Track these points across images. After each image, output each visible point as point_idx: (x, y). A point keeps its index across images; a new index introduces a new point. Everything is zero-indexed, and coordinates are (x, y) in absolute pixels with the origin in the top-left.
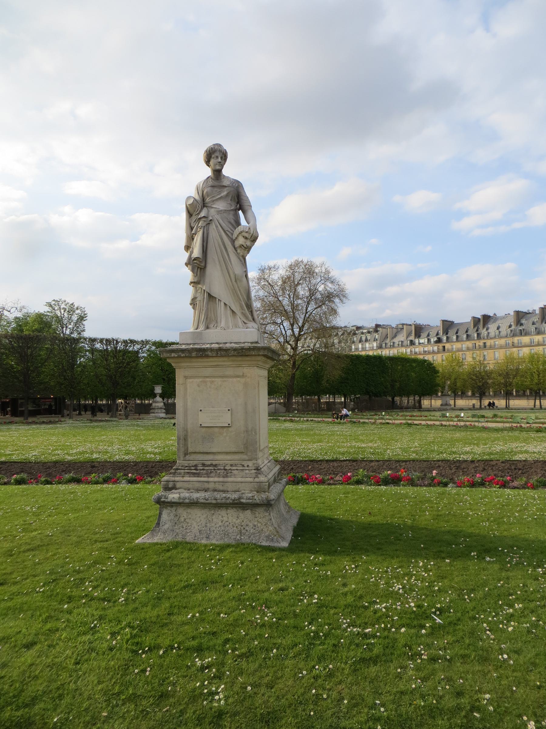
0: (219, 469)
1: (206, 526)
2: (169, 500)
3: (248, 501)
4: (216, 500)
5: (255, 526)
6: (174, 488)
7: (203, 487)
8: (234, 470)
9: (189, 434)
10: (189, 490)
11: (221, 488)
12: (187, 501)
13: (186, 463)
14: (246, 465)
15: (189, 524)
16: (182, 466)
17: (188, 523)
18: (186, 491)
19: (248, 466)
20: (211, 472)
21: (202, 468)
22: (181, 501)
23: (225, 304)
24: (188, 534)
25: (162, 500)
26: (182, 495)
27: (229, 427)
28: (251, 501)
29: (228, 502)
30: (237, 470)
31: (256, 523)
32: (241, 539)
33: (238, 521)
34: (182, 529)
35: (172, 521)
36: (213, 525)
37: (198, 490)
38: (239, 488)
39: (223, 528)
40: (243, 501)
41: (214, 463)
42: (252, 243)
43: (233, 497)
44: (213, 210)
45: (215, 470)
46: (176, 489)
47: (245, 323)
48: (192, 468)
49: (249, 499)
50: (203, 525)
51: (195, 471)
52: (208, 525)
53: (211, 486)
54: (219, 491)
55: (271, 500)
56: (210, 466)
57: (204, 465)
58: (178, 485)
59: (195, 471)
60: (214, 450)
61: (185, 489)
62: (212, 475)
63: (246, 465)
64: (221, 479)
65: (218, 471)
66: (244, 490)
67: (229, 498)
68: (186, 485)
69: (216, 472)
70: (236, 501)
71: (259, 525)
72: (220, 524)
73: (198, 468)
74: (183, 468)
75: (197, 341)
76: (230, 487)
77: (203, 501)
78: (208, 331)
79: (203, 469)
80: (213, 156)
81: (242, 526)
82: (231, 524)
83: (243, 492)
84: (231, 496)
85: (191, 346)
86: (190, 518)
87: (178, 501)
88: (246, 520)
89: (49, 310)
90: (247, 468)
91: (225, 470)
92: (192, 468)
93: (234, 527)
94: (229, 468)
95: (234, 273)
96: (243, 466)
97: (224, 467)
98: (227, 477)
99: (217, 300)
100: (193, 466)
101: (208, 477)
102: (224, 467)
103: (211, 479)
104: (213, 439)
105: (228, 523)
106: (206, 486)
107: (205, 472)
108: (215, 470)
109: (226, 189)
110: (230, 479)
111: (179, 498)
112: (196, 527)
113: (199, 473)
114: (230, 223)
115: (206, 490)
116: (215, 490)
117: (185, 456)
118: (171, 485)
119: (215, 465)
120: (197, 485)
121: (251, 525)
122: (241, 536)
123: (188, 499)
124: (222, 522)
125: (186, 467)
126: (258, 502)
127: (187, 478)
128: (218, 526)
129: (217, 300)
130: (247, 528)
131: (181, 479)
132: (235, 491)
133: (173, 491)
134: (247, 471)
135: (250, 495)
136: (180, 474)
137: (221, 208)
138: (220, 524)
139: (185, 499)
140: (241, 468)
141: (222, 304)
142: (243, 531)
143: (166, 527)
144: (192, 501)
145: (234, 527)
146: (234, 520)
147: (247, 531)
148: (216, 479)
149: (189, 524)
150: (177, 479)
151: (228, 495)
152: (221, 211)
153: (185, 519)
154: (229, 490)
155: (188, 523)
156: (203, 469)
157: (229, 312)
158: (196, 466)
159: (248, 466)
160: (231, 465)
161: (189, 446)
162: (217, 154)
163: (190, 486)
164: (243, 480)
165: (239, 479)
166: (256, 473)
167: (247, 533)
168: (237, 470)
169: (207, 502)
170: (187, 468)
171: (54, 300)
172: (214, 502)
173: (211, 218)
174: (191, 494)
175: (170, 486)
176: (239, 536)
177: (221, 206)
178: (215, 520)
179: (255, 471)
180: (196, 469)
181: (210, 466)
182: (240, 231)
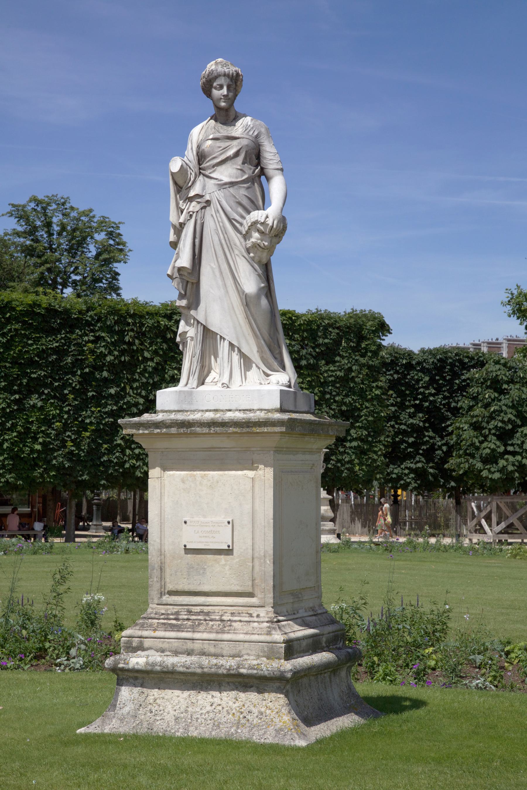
0: (211, 620)
1: (186, 711)
2: (131, 666)
3: (250, 671)
4: (202, 668)
5: (262, 714)
6: (141, 648)
7: (185, 647)
8: (235, 621)
9: (168, 561)
10: (163, 651)
11: (212, 650)
12: (158, 668)
13: (162, 609)
14: (255, 615)
15: (161, 708)
16: (156, 614)
17: (159, 706)
18: (159, 653)
19: (258, 616)
20: (199, 624)
21: (186, 617)
22: (149, 668)
23: (231, 345)
24: (158, 723)
25: (121, 666)
26: (151, 659)
27: (229, 551)
28: (255, 672)
29: (220, 671)
30: (240, 621)
31: (263, 710)
32: (237, 732)
33: (237, 704)
34: (149, 714)
35: (136, 702)
36: (198, 709)
37: (176, 653)
38: (240, 651)
39: (212, 715)
40: (243, 671)
41: (206, 609)
42: (275, 240)
43: (229, 664)
44: (213, 181)
45: (205, 620)
46: (144, 650)
47: (268, 375)
48: (171, 617)
49: (253, 669)
50: (182, 710)
51: (174, 622)
52: (190, 709)
53: (197, 646)
54: (209, 655)
55: (285, 672)
56: (198, 614)
57: (190, 612)
58: (147, 643)
59: (174, 622)
60: (206, 588)
61: (157, 651)
62: (202, 628)
63: (255, 615)
64: (213, 636)
65: (211, 623)
66: (248, 654)
67: (222, 665)
68: (158, 644)
69: (207, 624)
70: (232, 672)
71: (268, 712)
72: (209, 708)
73: (180, 617)
74: (157, 616)
75: (185, 407)
76: (226, 648)
77: (181, 669)
78: (201, 388)
79: (188, 619)
80: (215, 84)
81: (242, 713)
82: (225, 710)
83: (246, 657)
84: (224, 663)
85: (173, 416)
86: (163, 698)
87: (144, 668)
88: (249, 704)
89: (20, 229)
90: (255, 619)
91: (222, 621)
92: (171, 617)
93: (228, 713)
94: (228, 618)
95: (243, 292)
96: (251, 615)
97: (222, 616)
98: (223, 632)
99: (218, 336)
100: (172, 614)
101: (194, 632)
102: (222, 616)
103: (197, 636)
104: (205, 569)
105: (220, 708)
106: (190, 645)
107: (190, 623)
108: (205, 620)
109: (235, 142)
110: (226, 636)
111: (147, 663)
112: (172, 712)
113: (181, 625)
114: (240, 204)
115: (189, 653)
116: (203, 653)
117: (161, 597)
118: (135, 642)
119: (208, 614)
120: (176, 644)
121: (255, 711)
122: (238, 728)
123: (160, 666)
124: (211, 705)
125: (163, 614)
126: (266, 673)
127: (160, 633)
128: (204, 711)
129: (218, 336)
130: (248, 717)
131: (152, 634)
132: (233, 656)
133: (139, 652)
134: (256, 624)
135: (255, 662)
136: (151, 625)
137: (226, 179)
138: (209, 708)
139: (154, 664)
140: (247, 619)
141: (226, 343)
142: (243, 721)
143: (126, 709)
144: (165, 670)
145: (228, 713)
146: (231, 703)
147: (248, 720)
148: (205, 636)
149: (161, 708)
150: (145, 633)
151: (221, 661)
152: (226, 184)
153: (155, 700)
154: (224, 653)
155: (159, 706)
156: (188, 619)
157: (236, 357)
158: (177, 613)
159: (258, 616)
160: (233, 614)
161: (168, 580)
162: (222, 81)
163: (165, 646)
164: (247, 637)
165: (241, 637)
166: (269, 627)
167: (248, 725)
168: (240, 621)
169: (190, 670)
170: (162, 617)
171: (34, 199)
172: (199, 671)
173: (207, 198)
174: (165, 658)
175: (134, 644)
176: (235, 728)
177: (226, 174)
178: (200, 702)
179: (268, 625)
180: (177, 619)
181: (198, 614)
182: (253, 220)
